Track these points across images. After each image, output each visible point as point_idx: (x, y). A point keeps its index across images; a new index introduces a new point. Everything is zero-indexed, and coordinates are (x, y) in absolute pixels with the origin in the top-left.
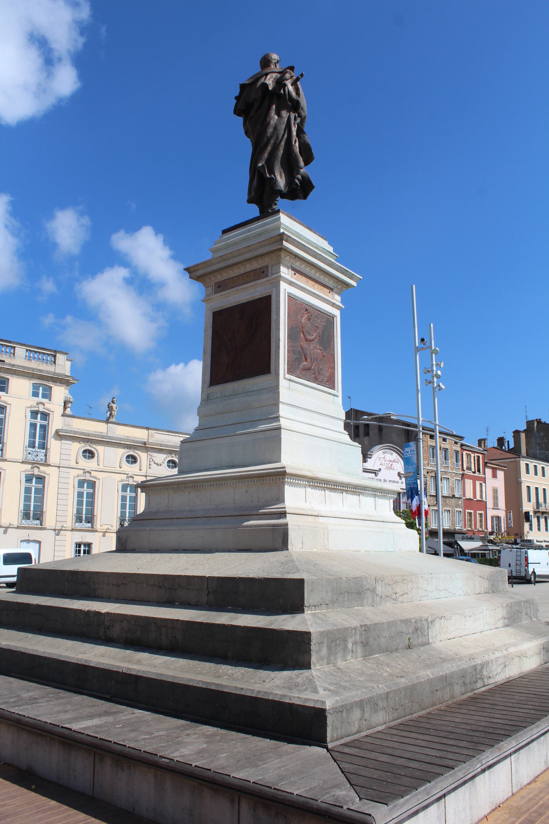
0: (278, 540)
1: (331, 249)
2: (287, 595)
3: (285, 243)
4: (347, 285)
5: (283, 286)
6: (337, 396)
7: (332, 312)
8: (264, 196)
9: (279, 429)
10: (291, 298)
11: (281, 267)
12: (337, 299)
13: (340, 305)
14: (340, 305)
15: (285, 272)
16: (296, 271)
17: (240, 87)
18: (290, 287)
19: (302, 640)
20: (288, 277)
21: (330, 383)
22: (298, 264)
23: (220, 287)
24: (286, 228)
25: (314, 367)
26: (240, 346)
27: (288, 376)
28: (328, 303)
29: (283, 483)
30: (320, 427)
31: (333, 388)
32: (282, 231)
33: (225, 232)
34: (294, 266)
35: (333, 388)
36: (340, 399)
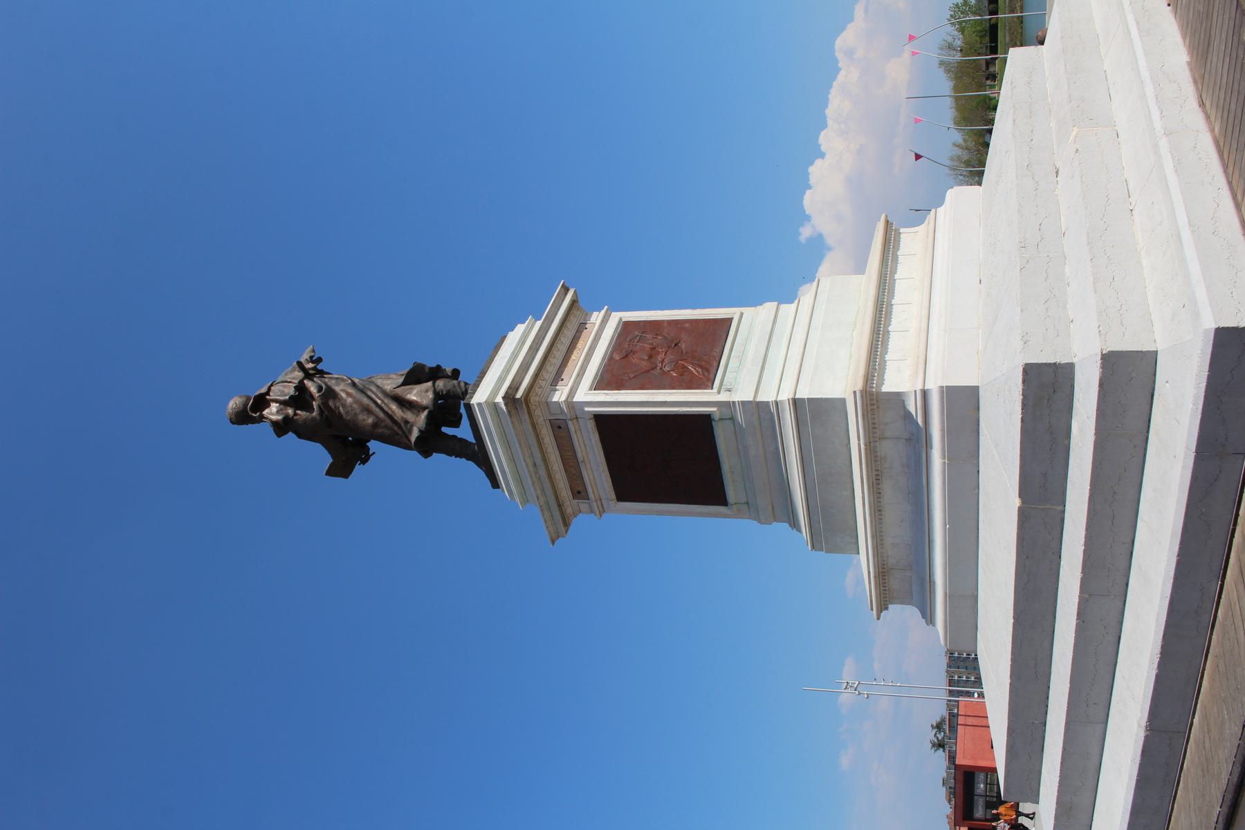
0: (963, 404)
1: (520, 328)
2: (1046, 388)
3: (519, 395)
4: (574, 303)
5: (579, 397)
6: (742, 314)
7: (614, 325)
8: (443, 426)
9: (796, 403)
10: (609, 379)
11: (555, 399)
12: (596, 318)
13: (603, 312)
14: (603, 312)
15: (560, 396)
16: (558, 378)
17: (1055, 366)
18: (582, 389)
19: (1113, 364)
20: (566, 390)
21: (726, 323)
22: (549, 375)
23: (579, 492)
24: (495, 392)
25: (699, 350)
26: (670, 461)
27: (715, 390)
28: (603, 330)
29: (879, 393)
30: (767, 349)
31: (730, 320)
32: (499, 399)
33: (495, 484)
34: (550, 381)
35: (730, 320)
36: (745, 310)
